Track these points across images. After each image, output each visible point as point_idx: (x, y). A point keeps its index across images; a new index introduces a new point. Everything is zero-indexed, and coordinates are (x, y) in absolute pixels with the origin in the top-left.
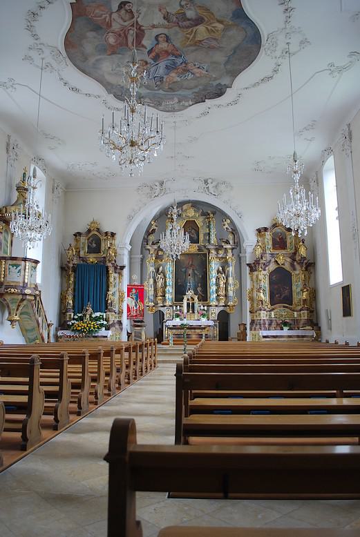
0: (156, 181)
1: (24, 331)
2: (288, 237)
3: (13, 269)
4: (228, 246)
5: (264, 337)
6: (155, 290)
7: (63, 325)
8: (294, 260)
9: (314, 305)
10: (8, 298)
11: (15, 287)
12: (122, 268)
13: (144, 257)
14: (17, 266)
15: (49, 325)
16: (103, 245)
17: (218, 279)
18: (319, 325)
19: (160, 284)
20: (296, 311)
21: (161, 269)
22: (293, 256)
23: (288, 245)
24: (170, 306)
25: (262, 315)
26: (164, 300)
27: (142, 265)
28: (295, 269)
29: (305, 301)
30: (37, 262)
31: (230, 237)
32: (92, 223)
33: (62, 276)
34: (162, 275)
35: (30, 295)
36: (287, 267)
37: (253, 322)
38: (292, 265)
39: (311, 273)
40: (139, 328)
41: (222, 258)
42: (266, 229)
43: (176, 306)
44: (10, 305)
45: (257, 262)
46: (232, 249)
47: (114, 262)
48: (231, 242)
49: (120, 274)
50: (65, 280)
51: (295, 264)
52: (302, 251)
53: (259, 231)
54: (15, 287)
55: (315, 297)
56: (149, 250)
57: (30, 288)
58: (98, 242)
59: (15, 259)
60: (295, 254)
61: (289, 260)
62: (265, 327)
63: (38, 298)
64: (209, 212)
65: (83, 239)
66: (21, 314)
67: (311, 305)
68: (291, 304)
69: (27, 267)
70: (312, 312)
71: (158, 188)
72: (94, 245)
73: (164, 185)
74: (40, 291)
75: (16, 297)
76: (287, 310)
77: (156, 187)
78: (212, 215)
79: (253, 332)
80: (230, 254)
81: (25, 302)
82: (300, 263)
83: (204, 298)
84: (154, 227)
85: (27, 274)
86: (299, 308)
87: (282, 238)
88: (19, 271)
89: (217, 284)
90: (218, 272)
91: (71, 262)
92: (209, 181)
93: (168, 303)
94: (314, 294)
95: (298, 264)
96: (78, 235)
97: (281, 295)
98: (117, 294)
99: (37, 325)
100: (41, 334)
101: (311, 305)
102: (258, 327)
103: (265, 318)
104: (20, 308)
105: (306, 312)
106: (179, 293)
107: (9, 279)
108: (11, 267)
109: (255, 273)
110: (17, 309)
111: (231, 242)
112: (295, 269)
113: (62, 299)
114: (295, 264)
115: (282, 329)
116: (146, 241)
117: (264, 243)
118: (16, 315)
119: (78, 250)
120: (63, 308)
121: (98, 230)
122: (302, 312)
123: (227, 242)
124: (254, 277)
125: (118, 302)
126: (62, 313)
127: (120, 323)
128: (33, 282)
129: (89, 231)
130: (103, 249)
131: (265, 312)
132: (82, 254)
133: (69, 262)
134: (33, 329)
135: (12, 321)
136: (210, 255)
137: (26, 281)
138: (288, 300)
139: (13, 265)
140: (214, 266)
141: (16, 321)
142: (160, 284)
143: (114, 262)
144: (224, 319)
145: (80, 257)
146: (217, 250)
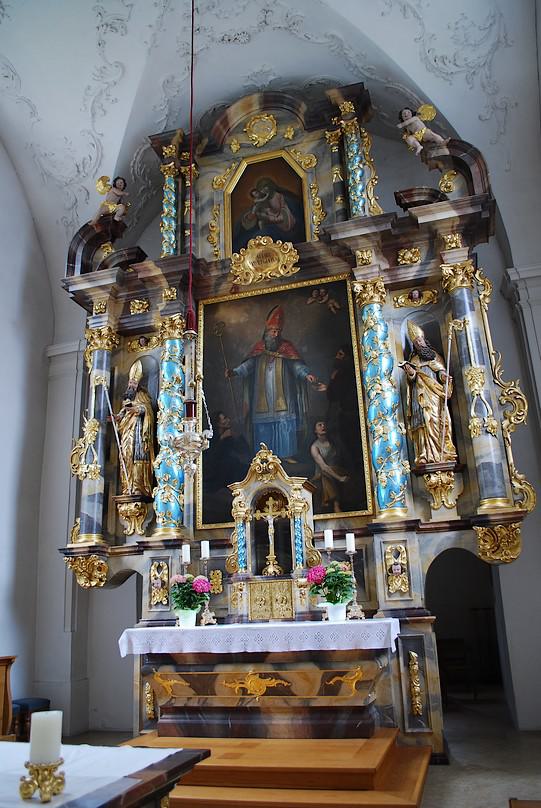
89: (410, 414)
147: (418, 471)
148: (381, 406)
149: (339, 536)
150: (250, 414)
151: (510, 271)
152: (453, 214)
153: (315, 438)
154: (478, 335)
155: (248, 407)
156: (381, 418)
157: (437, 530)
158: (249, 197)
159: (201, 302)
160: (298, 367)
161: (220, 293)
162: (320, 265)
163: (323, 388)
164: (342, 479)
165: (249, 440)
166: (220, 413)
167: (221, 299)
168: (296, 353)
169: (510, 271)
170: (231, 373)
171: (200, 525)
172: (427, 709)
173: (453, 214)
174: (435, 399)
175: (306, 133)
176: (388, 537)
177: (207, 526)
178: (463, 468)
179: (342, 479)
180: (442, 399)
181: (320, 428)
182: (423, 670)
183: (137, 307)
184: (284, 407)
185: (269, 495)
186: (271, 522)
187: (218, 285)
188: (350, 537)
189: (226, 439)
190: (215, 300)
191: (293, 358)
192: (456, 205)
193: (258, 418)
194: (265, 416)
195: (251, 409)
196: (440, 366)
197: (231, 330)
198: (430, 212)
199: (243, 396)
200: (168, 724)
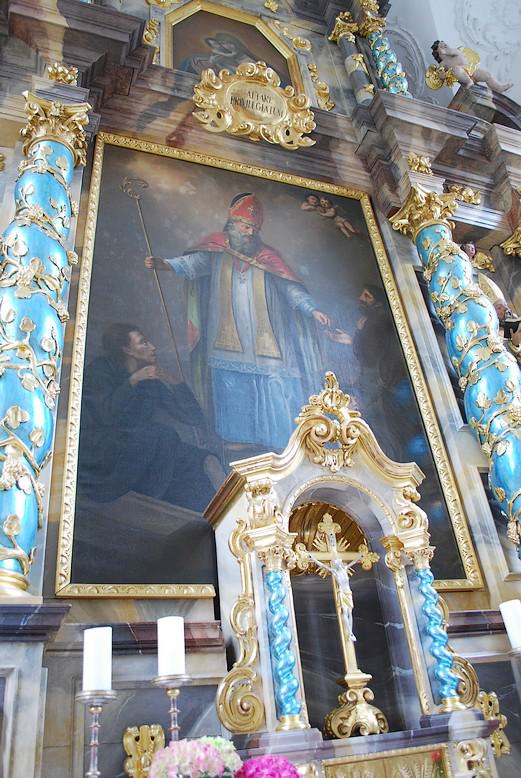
150: (202, 346)
155: (198, 333)
158: (206, 45)
160: (295, 293)
161: (146, 132)
162: (329, 160)
165: (201, 399)
166: (134, 328)
167: (144, 147)
168: (289, 269)
170: (158, 264)
171: (64, 586)
175: (294, 16)
177: (89, 590)
183: (188, 82)
184: (276, 353)
185: (325, 509)
186: (342, 576)
187: (149, 117)
189: (144, 384)
190: (133, 144)
191: (285, 276)
193: (218, 359)
194: (235, 358)
195: (204, 338)
197: (159, 197)
199: (184, 311)
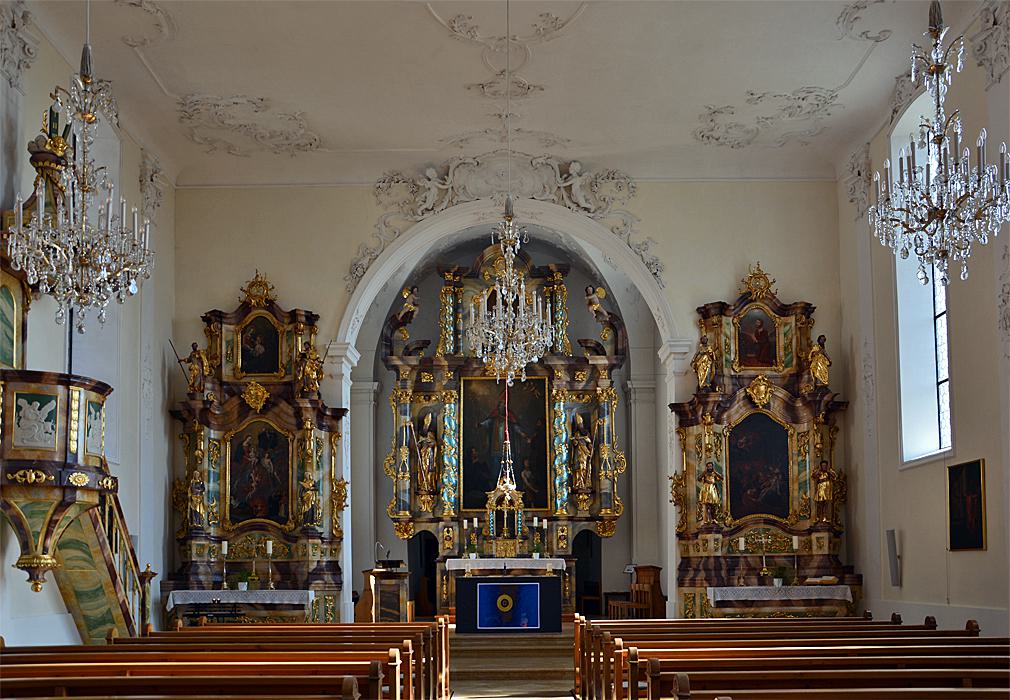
0: (430, 165)
1: (72, 599)
2: (781, 331)
3: (31, 411)
4: (602, 361)
5: (721, 604)
6: (413, 478)
7: (179, 573)
8: (794, 394)
9: (842, 519)
10: (18, 502)
11: (39, 465)
12: (339, 413)
13: (381, 388)
14: (44, 400)
15: (145, 578)
16: (284, 348)
17: (573, 447)
18: (857, 572)
19: (426, 460)
20: (798, 533)
21: (428, 421)
22: (792, 384)
23: (780, 353)
24: (453, 519)
25: (711, 545)
26: (438, 504)
27: (377, 407)
28: (796, 420)
29: (822, 505)
30: (102, 389)
31: (607, 335)
32: (252, 285)
33: (172, 436)
34: (429, 438)
35: (86, 489)
36: (777, 412)
37: (685, 565)
38: (789, 407)
39: (837, 430)
40: (393, 582)
41: (585, 391)
42: (722, 308)
43: (470, 521)
44: (27, 522)
45: (702, 395)
46: (610, 368)
47: (316, 397)
48: (608, 349)
49: (334, 432)
50: (180, 447)
51: (799, 404)
52: (820, 370)
53: (705, 313)
54: (39, 465)
55: (844, 496)
56: (396, 368)
57: (85, 469)
58: (271, 338)
59: (37, 377)
60: (797, 377)
61: (781, 394)
62: (719, 576)
63: (110, 498)
64: (553, 267)
65: (227, 329)
66: (61, 546)
67: (835, 517)
68: (785, 515)
69: (75, 405)
70: (837, 534)
71: (434, 186)
72: (260, 349)
73: (449, 179)
74: (115, 480)
75: (42, 495)
76: (773, 529)
77: (428, 184)
78: (558, 276)
79: (686, 590)
80: (604, 383)
81: (71, 512)
82: (812, 404)
83: (536, 494)
84: (409, 306)
85: (74, 425)
86: (807, 524)
87: (764, 332)
88: (51, 416)
89: (572, 463)
90: (574, 427)
91: (198, 396)
92: (574, 168)
93: (449, 511)
94: (843, 487)
95: (807, 404)
96: (213, 318)
97: (759, 490)
98: (326, 488)
99: (107, 577)
100: (123, 606)
101: (835, 517)
102: (702, 575)
103: (719, 554)
104: (57, 531)
105: (825, 535)
106: (478, 483)
107: (17, 439)
108: (22, 402)
109: (695, 430)
110: (48, 534)
111: (608, 349)
112: (796, 420)
113: (178, 499)
114: (799, 404)
115: (762, 581)
116: (387, 343)
117: (717, 348)
118: (45, 551)
119: (216, 363)
120: (178, 527)
121: (271, 305)
122: (814, 536)
123: (598, 350)
124: (691, 440)
125: (327, 511)
126: (180, 531)
127: (335, 568)
128: (93, 451)
129: (245, 307)
130: (283, 359)
131: (720, 536)
132: (227, 372)
133: (192, 396)
134: (98, 591)
135: (34, 573)
136: (556, 383)
137: (73, 447)
138: (777, 504)
139: (31, 398)
140: (562, 417)
141: (46, 569)
142: (426, 460)
143: (316, 397)
144: (586, 548)
145: (222, 383)
146: (571, 370)
147: (574, 492)
148: (561, 479)
149: (540, 520)
151: (628, 382)
152: (606, 362)
153: (523, 468)
154: (608, 428)
156: (560, 466)
157: (580, 521)
159: (462, 379)
160: (516, 427)
163: (529, 441)
164: (536, 491)
169: (628, 382)
172: (570, 597)
173: (606, 362)
174: (585, 458)
176: (560, 523)
178: (594, 492)
179: (536, 491)
180: (588, 458)
181: (526, 463)
182: (570, 581)
188: (545, 521)
192: (608, 358)
196: (589, 440)
197: (479, 399)
198: (596, 359)
200: (231, 446)
